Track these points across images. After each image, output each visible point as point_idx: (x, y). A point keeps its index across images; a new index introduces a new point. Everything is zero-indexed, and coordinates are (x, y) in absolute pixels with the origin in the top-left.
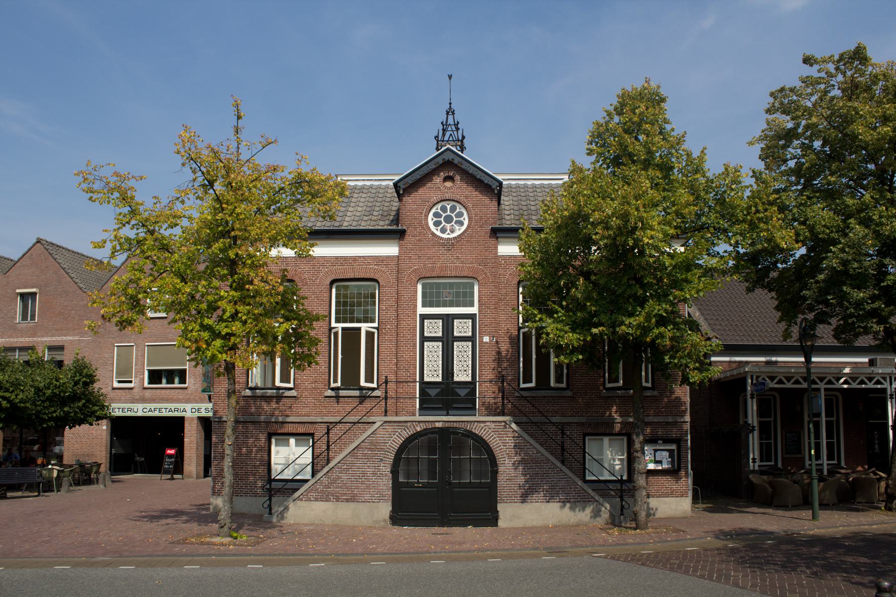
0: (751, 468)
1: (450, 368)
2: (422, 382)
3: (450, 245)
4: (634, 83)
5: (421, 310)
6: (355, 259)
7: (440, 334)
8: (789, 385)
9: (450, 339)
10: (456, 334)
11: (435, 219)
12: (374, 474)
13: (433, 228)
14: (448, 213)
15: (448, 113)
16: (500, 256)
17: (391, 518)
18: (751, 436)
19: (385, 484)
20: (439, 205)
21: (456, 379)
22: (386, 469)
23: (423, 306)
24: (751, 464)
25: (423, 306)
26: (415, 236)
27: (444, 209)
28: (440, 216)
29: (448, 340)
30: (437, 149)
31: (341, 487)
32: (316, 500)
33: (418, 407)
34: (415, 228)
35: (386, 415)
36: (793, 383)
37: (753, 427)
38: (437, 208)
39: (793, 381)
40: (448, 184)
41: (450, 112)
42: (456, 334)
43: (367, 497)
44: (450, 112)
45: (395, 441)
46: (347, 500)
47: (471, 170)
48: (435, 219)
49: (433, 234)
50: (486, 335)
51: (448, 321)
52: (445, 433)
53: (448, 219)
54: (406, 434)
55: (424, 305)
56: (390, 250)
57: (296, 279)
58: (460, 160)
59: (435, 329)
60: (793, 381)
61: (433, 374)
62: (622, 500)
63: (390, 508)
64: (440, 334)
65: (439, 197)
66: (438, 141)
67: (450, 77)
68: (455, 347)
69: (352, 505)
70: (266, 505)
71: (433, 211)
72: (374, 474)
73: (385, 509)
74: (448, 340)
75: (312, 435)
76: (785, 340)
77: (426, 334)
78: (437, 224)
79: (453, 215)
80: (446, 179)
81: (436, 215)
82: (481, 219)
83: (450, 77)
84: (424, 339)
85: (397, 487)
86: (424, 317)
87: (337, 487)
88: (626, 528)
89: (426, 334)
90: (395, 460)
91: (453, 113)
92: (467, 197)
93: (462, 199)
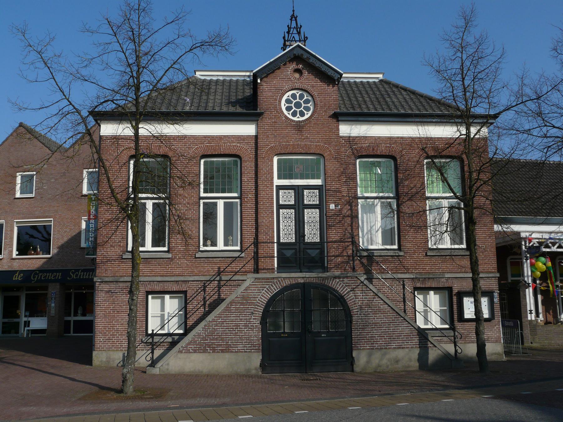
0: (529, 319)
1: (302, 231)
2: (279, 242)
3: (299, 126)
5: (277, 182)
6: (220, 138)
7: (293, 203)
9: (301, 207)
10: (306, 202)
11: (287, 105)
12: (246, 326)
13: (285, 112)
14: (298, 100)
15: (291, 20)
16: (341, 137)
17: (261, 365)
18: (527, 290)
19: (256, 335)
20: (300, 92)
22: (256, 322)
23: (278, 178)
24: (529, 315)
25: (278, 178)
26: (271, 118)
28: (291, 102)
29: (299, 207)
30: (284, 47)
31: (216, 339)
32: (195, 351)
33: (276, 266)
34: (271, 112)
35: (258, 273)
37: (529, 284)
38: (298, 93)
40: (297, 75)
41: (293, 17)
42: (306, 202)
43: (240, 347)
44: (293, 17)
45: (263, 296)
46: (222, 351)
47: (318, 64)
48: (287, 105)
49: (286, 117)
50: (333, 203)
51: (299, 191)
52: (304, 287)
53: (298, 105)
54: (275, 289)
55: (279, 178)
56: (248, 129)
57: (170, 154)
58: (308, 55)
59: (288, 198)
61: (288, 235)
62: (455, 346)
63: (261, 357)
64: (293, 203)
66: (285, 41)
68: (306, 213)
69: (227, 355)
72: (246, 326)
73: (256, 359)
74: (299, 207)
75: (185, 293)
77: (281, 203)
79: (302, 102)
80: (297, 71)
82: (325, 105)
84: (280, 207)
85: (265, 337)
86: (279, 188)
87: (213, 339)
89: (281, 203)
90: (263, 313)
92: (313, 87)
93: (309, 88)
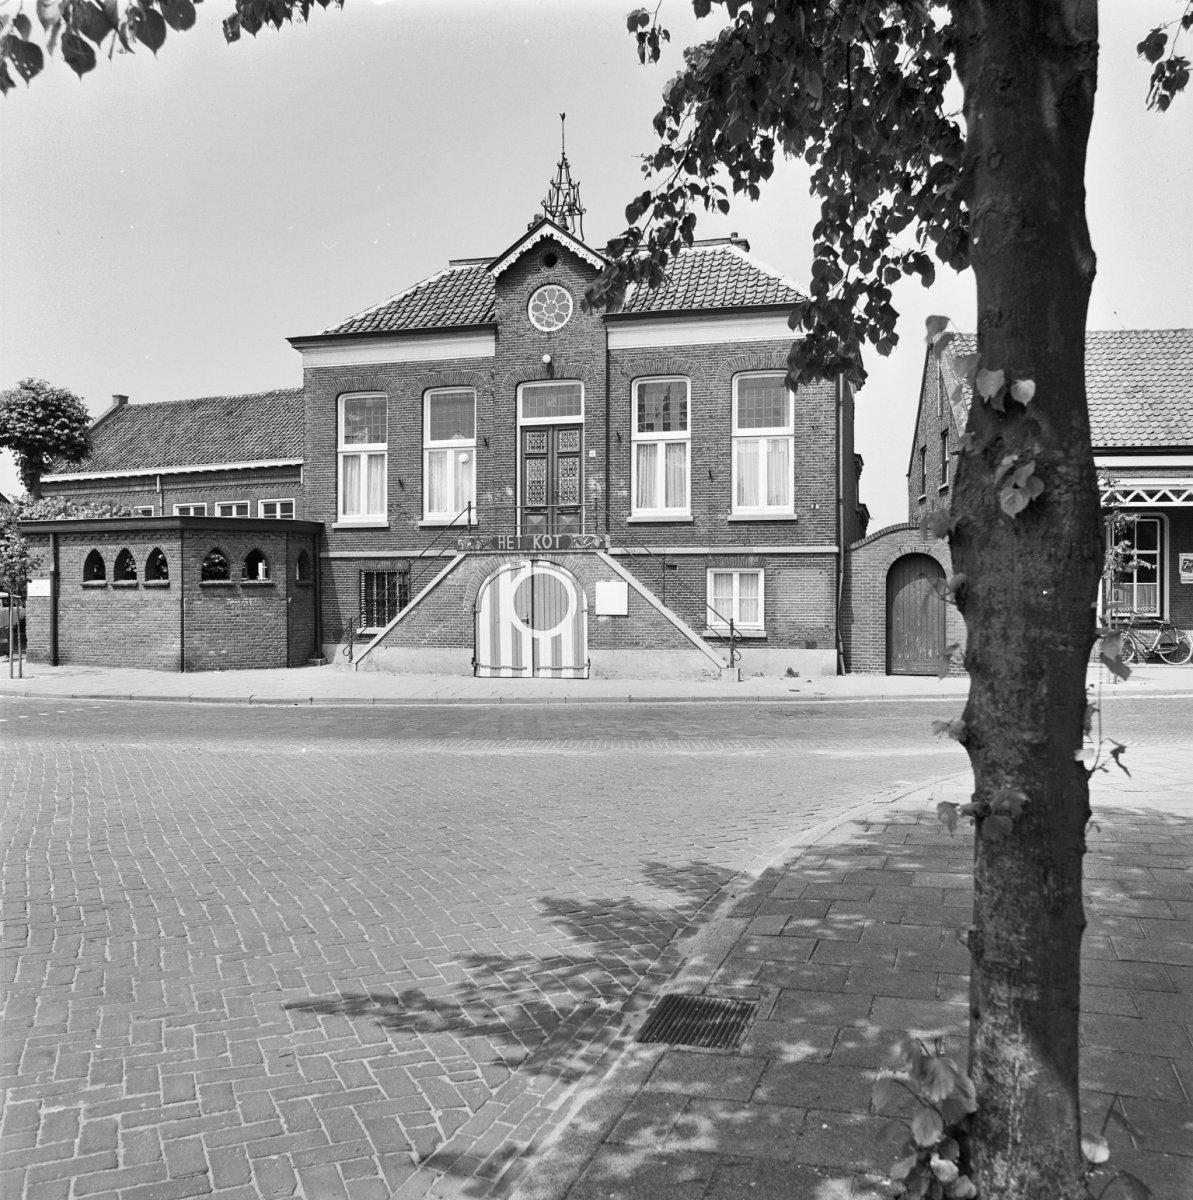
4: (761, 196)
5: (522, 421)
8: (1151, 503)
15: (560, 167)
21: (1094, 444)
23: (432, 439)
25: (432, 439)
27: (541, 298)
36: (1158, 500)
39: (1184, 496)
41: (564, 165)
44: (564, 165)
60: (1184, 496)
65: (526, 294)
67: (563, 117)
70: (347, 652)
71: (531, 305)
76: (157, 551)
78: (539, 320)
81: (537, 308)
83: (563, 117)
86: (525, 429)
88: (182, 600)
91: (567, 167)
